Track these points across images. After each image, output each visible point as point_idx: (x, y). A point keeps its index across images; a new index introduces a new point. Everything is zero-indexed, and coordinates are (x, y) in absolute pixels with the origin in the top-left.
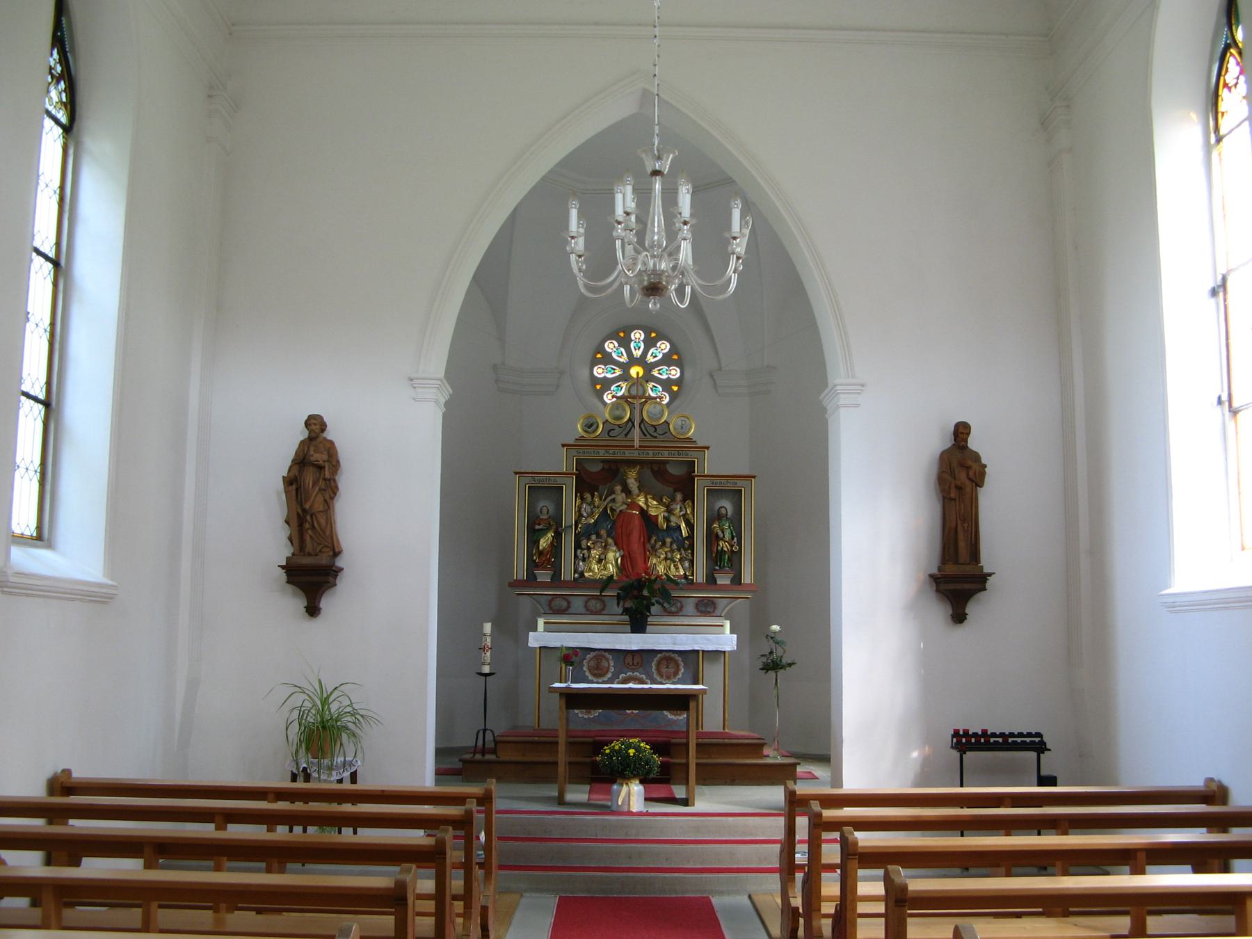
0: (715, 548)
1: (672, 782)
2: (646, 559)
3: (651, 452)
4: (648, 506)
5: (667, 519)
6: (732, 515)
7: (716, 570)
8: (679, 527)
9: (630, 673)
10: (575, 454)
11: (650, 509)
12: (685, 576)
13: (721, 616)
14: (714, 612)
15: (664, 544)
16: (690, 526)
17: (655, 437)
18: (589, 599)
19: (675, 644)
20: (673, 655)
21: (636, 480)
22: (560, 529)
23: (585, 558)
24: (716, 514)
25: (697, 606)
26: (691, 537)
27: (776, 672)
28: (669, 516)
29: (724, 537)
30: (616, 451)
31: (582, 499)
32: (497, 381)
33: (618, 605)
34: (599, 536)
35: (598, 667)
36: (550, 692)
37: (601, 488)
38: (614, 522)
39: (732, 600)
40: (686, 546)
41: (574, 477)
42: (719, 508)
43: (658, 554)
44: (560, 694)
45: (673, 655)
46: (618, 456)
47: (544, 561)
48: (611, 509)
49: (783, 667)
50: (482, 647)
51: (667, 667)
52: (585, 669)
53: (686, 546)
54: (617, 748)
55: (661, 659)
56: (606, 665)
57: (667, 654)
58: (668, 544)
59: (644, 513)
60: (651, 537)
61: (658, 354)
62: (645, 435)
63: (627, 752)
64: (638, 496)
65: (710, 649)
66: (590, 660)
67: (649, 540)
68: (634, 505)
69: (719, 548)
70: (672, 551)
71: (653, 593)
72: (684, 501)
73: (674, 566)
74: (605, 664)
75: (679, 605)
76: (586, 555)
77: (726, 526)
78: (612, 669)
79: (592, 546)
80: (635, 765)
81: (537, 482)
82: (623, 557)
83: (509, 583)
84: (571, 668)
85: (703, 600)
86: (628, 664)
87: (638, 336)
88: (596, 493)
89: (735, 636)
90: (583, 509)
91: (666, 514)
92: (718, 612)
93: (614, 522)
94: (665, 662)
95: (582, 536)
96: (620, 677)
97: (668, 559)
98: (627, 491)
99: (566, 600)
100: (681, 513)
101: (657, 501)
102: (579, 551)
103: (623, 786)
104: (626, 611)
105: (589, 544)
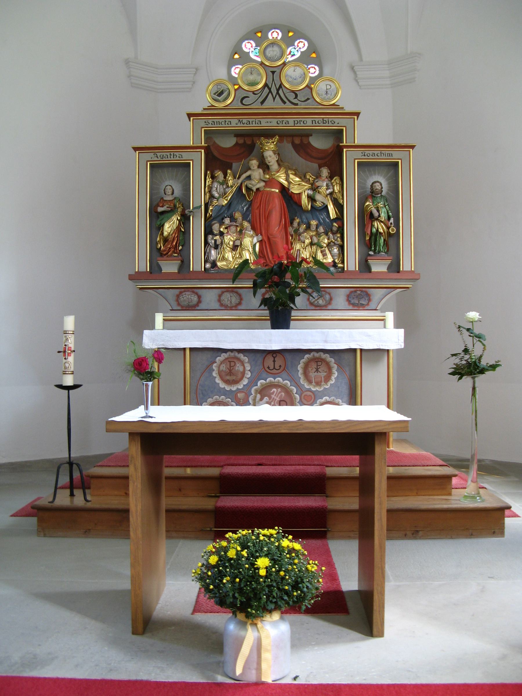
0: (369, 229)
1: (329, 535)
2: (289, 245)
3: (291, 122)
4: (289, 183)
5: (312, 199)
6: (387, 193)
7: (370, 255)
8: (326, 207)
9: (270, 379)
10: (203, 124)
11: (291, 186)
12: (335, 264)
13: (376, 310)
14: (368, 304)
15: (308, 227)
16: (339, 207)
17: (297, 104)
18: (223, 292)
19: (326, 342)
20: (323, 356)
21: (274, 152)
22: (186, 212)
23: (218, 245)
24: (369, 190)
25: (348, 298)
26: (340, 218)
27: (473, 378)
28: (314, 194)
29: (379, 216)
30: (251, 120)
31: (213, 177)
32: (129, 76)
33: (254, 295)
34: (233, 219)
35: (230, 372)
36: (108, 431)
37: (234, 165)
38: (251, 204)
39: (392, 290)
40: (335, 229)
41: (203, 151)
42: (373, 183)
43: (302, 238)
44: (131, 434)
45: (323, 356)
46: (254, 126)
47: (170, 248)
48: (247, 188)
49: (482, 371)
50: (62, 350)
51: (317, 370)
52: (214, 374)
53: (335, 229)
54: (232, 554)
55: (310, 361)
56: (241, 369)
57: (317, 355)
58: (313, 228)
59: (284, 190)
60: (294, 219)
61: (296, 53)
62: (284, 103)
63: (253, 565)
64: (278, 172)
65: (371, 348)
66: (221, 363)
67: (292, 223)
68: (271, 182)
69: (374, 230)
70: (318, 235)
71: (297, 278)
72: (331, 177)
73: (322, 252)
74: (239, 368)
75: (327, 297)
76: (218, 242)
77: (381, 205)
78: (248, 375)
79: (226, 231)
80: (271, 592)
81: (159, 159)
82: (261, 242)
83: (130, 275)
84: (150, 384)
85: (355, 291)
86: (268, 368)
87: (275, 35)
88: (229, 171)
89: (402, 331)
90: (214, 189)
91: (310, 192)
92: (372, 305)
93: (251, 204)
94: (314, 365)
95: (214, 219)
96: (259, 384)
97: (315, 244)
98: (264, 166)
99: (197, 294)
100: (328, 191)
101: (300, 178)
102: (210, 237)
103: (247, 630)
104: (265, 302)
105: (222, 230)
